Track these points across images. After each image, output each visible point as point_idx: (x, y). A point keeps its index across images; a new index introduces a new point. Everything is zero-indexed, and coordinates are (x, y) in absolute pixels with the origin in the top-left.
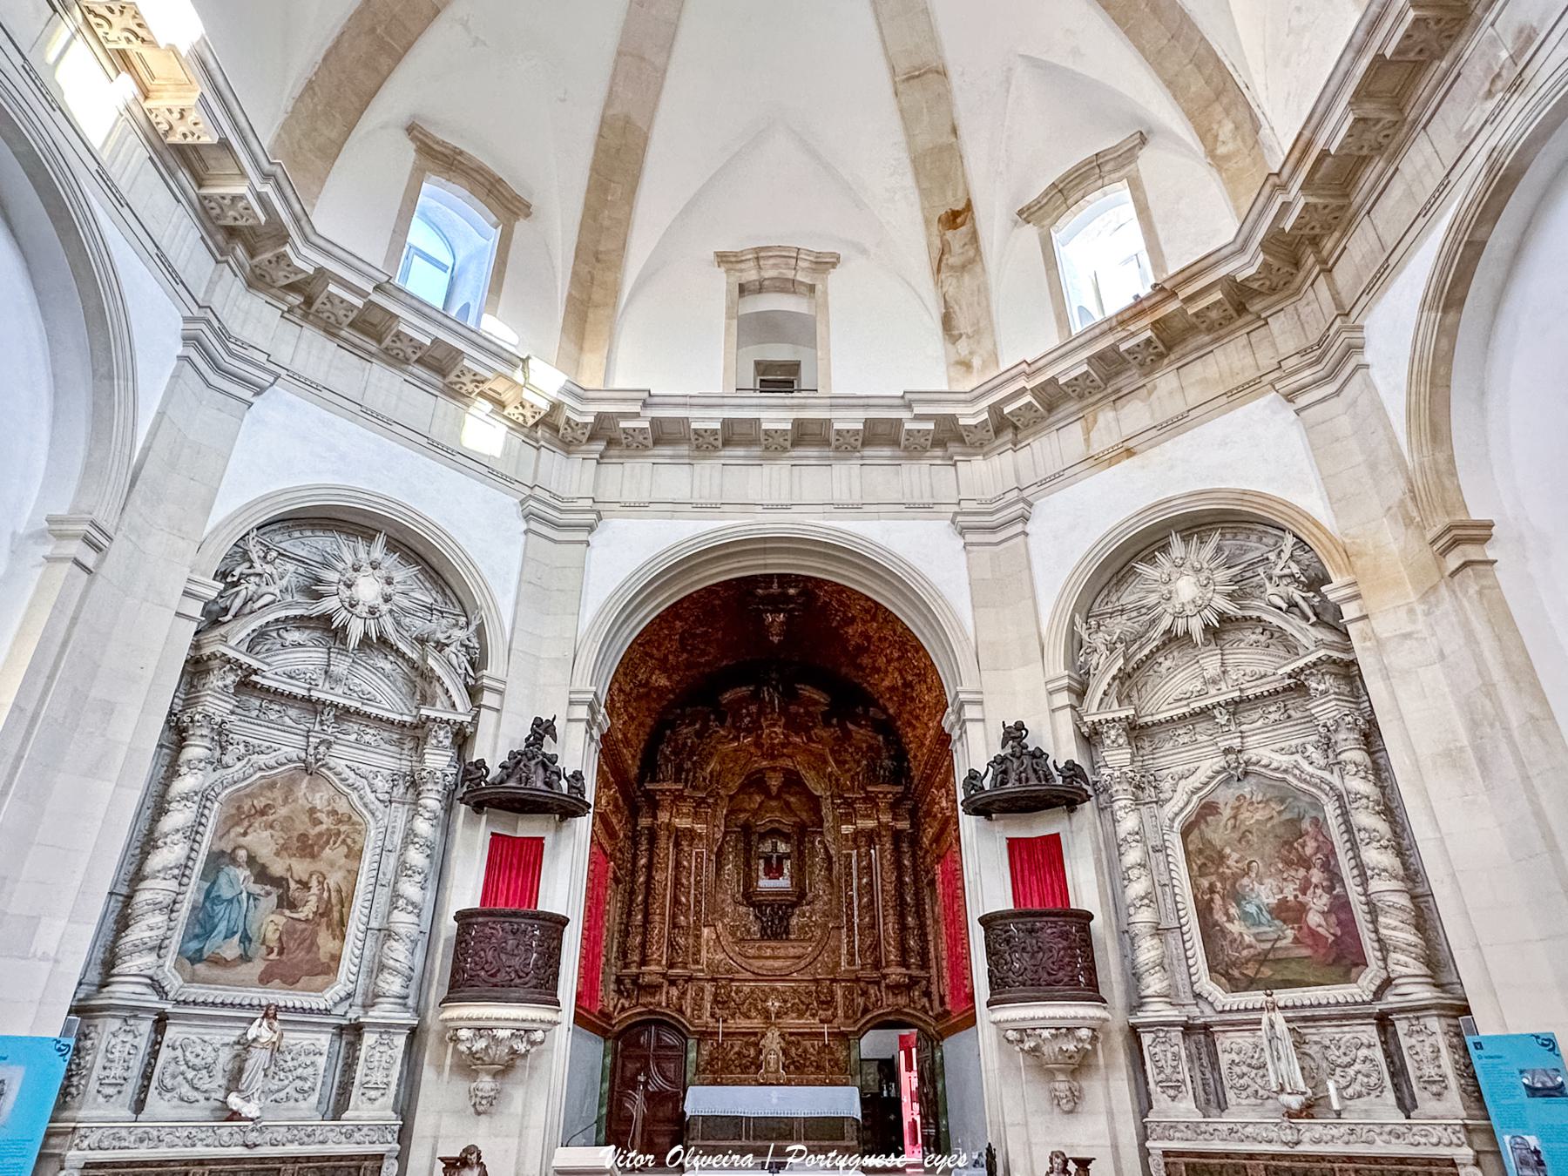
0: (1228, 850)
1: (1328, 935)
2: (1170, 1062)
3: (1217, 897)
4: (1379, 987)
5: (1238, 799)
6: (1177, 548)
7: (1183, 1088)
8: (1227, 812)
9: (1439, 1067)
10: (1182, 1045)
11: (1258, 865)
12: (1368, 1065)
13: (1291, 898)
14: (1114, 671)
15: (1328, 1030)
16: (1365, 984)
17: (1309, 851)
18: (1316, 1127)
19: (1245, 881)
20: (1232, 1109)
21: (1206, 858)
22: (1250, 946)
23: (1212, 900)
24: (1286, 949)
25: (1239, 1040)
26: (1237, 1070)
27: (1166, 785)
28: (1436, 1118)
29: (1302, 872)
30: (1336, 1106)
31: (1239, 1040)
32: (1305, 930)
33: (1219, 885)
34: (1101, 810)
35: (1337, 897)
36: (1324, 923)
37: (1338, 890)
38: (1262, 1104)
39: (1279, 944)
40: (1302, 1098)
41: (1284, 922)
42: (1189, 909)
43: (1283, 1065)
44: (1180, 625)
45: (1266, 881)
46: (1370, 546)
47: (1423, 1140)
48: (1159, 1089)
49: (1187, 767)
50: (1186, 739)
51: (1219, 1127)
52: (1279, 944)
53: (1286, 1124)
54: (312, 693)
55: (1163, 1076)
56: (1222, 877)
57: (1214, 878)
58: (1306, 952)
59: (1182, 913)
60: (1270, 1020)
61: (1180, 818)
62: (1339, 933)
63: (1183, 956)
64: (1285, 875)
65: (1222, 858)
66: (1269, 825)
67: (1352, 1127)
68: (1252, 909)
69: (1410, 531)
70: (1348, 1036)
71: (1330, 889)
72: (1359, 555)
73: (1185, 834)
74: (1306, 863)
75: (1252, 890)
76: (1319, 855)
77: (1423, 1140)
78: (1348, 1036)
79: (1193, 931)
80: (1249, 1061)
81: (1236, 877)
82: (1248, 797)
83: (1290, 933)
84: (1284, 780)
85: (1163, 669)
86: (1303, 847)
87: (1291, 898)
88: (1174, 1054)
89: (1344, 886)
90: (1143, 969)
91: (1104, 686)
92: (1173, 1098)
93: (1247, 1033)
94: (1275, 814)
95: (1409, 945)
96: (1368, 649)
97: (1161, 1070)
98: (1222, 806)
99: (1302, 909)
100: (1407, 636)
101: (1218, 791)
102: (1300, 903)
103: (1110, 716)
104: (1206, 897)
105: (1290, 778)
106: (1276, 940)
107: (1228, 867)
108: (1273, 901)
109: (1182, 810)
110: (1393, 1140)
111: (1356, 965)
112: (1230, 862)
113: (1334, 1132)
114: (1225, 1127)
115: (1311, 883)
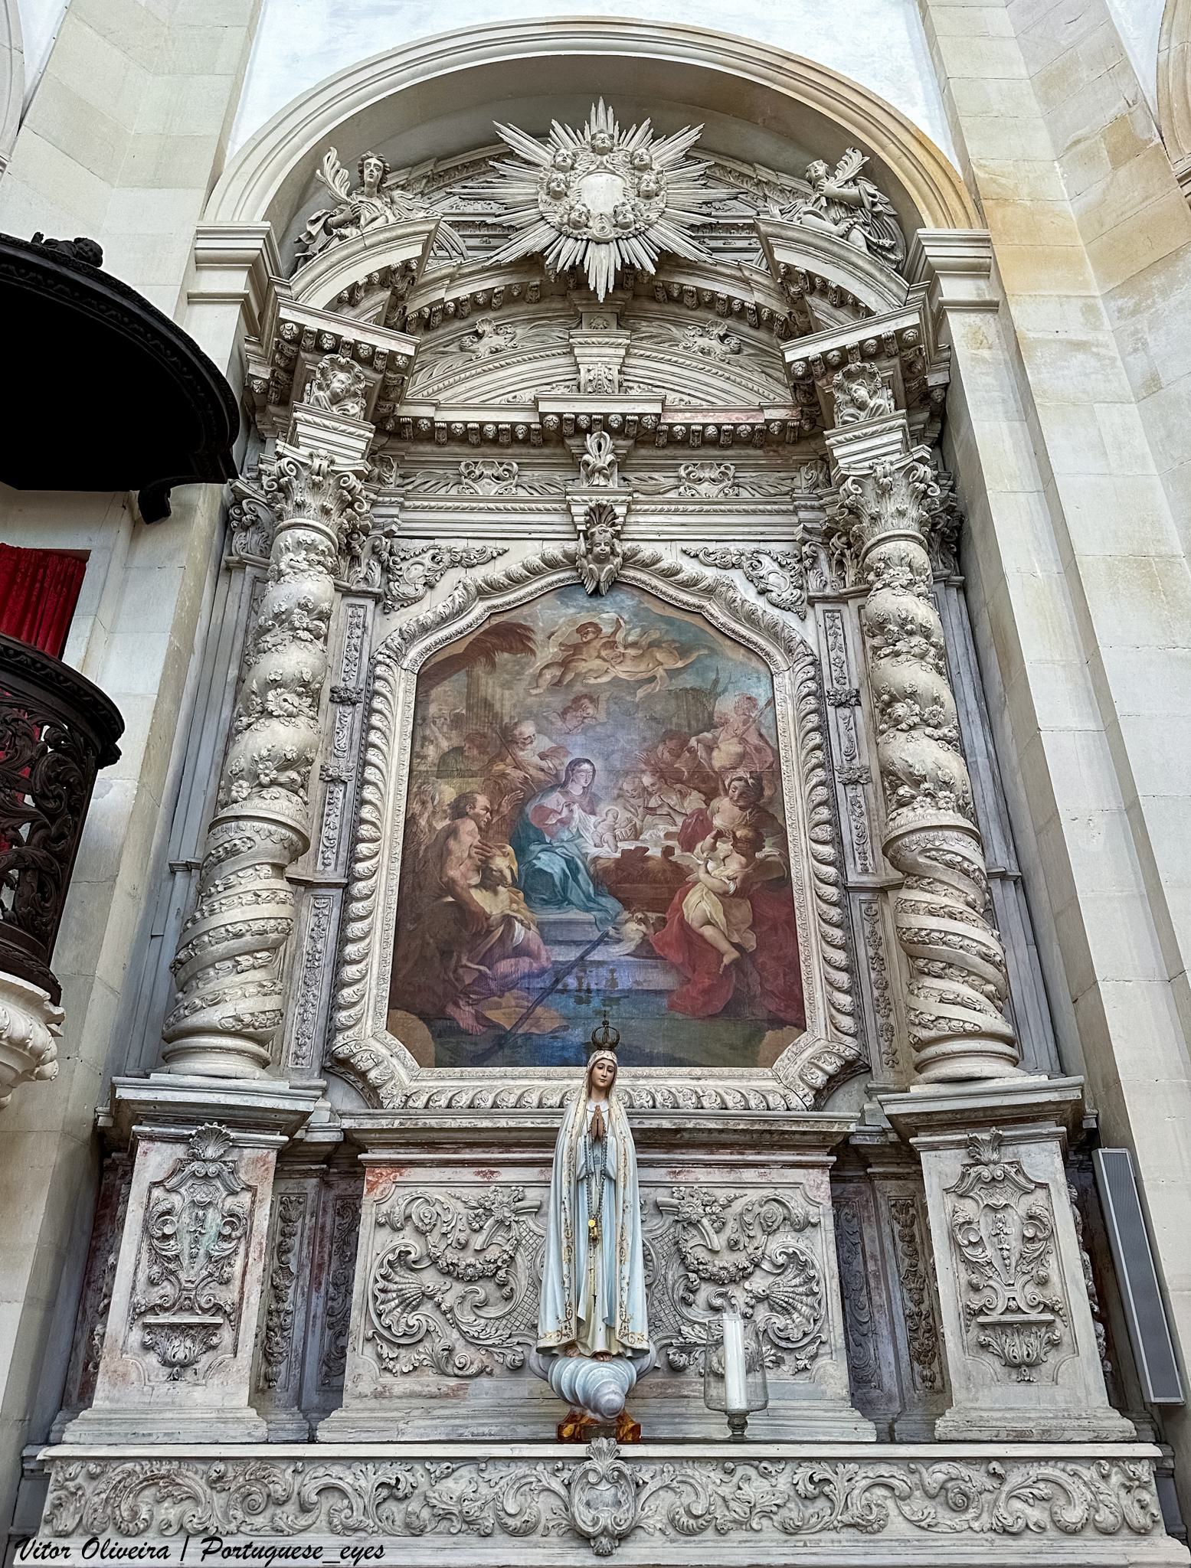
0: (528, 729)
1: (724, 946)
2: (207, 1243)
3: (468, 826)
4: (831, 1078)
5: (582, 630)
6: (602, 121)
7: (226, 1336)
8: (548, 652)
9: (1043, 1282)
10: (266, 1192)
11: (594, 773)
12: (791, 1279)
13: (655, 852)
14: (394, 258)
15: (701, 1175)
16: (794, 1070)
17: (720, 759)
18: (698, 1474)
19: (553, 800)
20: (351, 1408)
21: (469, 738)
22: (521, 951)
23: (452, 832)
24: (613, 967)
25: (435, 1193)
26: (408, 1283)
27: (414, 573)
28: (1021, 1439)
29: (694, 801)
30: (736, 1393)
31: (435, 1193)
32: (674, 927)
33: (482, 801)
34: (226, 569)
35: (765, 865)
36: (720, 919)
37: (768, 850)
38: (453, 1394)
39: (596, 956)
40: (627, 1371)
41: (627, 904)
42: (385, 844)
43: (597, 1265)
44: (568, 252)
45: (604, 807)
46: (1025, 191)
47: (1036, 1514)
48: (136, 1336)
49: (478, 545)
50: (492, 489)
51: (346, 1478)
52: (596, 956)
53: (602, 1465)
54: (544, 407)
55: (167, 1289)
56: (498, 788)
57: (474, 784)
58: (659, 979)
59: (363, 848)
60: (597, 1120)
61: (430, 640)
62: (751, 943)
63: (326, 960)
64: (653, 803)
65: (508, 739)
66: (640, 693)
67: (822, 1472)
68: (551, 864)
69: (1122, 173)
70: (753, 1195)
71: (749, 847)
72: (1002, 201)
73: (427, 678)
74: (710, 786)
75: (564, 823)
76: (741, 772)
77: (1036, 1514)
78: (753, 1195)
79: (380, 897)
80: (451, 1256)
81: (534, 789)
82: (607, 630)
83: (634, 930)
84: (697, 612)
85: (483, 347)
86: (710, 749)
87: (655, 852)
88: (232, 1218)
89: (783, 845)
90: (220, 948)
91: (358, 274)
92: (177, 1369)
93: (468, 1174)
94: (660, 672)
95: (986, 958)
96: (984, 361)
97: (166, 1266)
98: (539, 637)
99: (678, 879)
100: (1079, 346)
101: (538, 607)
102: (676, 866)
103: (350, 335)
104: (441, 825)
105: (713, 608)
106: (595, 944)
107: (518, 766)
108: (609, 853)
109: (443, 620)
110: (946, 1518)
111: (777, 1023)
112: (528, 755)
113: (756, 1489)
114: (367, 1480)
115: (709, 827)
